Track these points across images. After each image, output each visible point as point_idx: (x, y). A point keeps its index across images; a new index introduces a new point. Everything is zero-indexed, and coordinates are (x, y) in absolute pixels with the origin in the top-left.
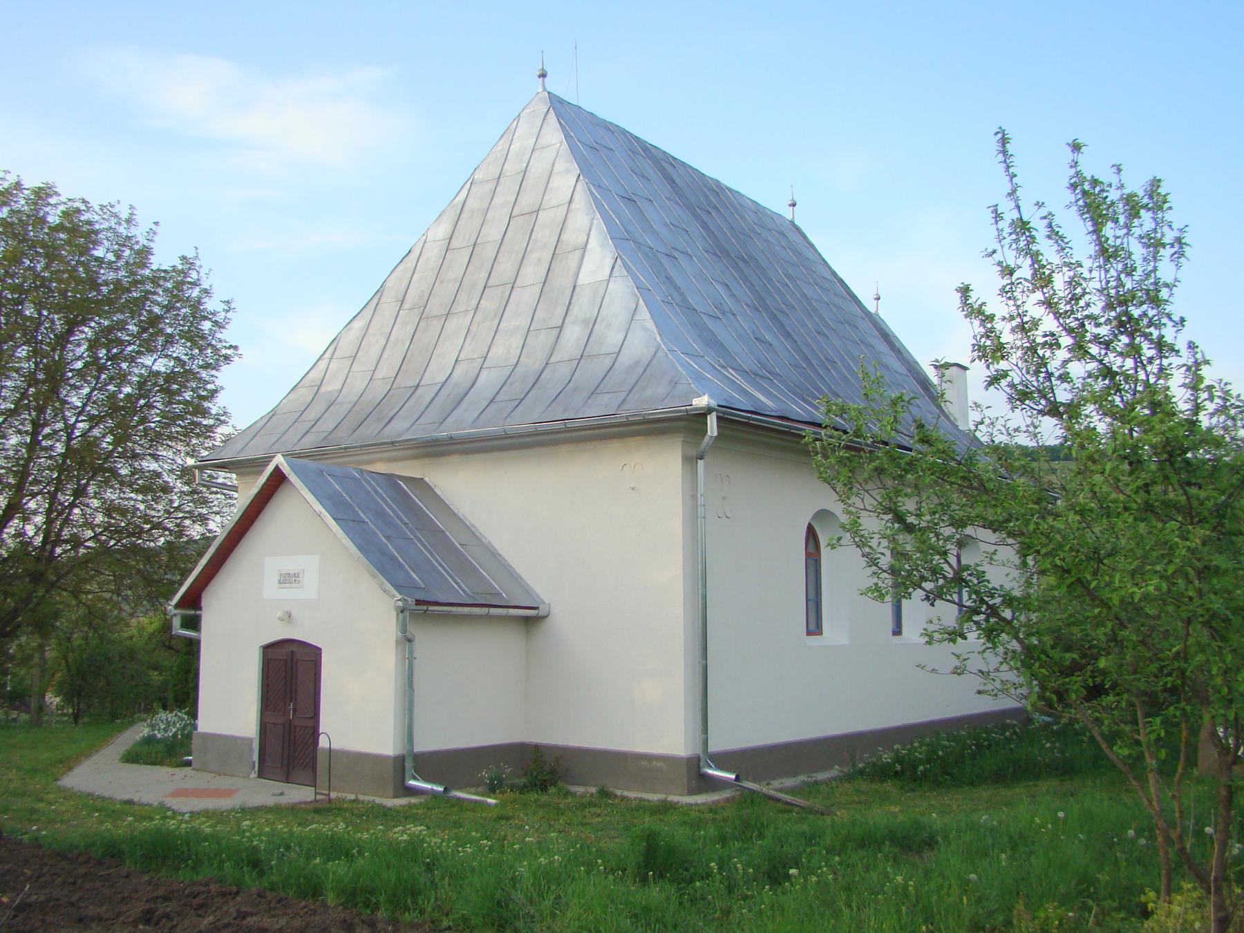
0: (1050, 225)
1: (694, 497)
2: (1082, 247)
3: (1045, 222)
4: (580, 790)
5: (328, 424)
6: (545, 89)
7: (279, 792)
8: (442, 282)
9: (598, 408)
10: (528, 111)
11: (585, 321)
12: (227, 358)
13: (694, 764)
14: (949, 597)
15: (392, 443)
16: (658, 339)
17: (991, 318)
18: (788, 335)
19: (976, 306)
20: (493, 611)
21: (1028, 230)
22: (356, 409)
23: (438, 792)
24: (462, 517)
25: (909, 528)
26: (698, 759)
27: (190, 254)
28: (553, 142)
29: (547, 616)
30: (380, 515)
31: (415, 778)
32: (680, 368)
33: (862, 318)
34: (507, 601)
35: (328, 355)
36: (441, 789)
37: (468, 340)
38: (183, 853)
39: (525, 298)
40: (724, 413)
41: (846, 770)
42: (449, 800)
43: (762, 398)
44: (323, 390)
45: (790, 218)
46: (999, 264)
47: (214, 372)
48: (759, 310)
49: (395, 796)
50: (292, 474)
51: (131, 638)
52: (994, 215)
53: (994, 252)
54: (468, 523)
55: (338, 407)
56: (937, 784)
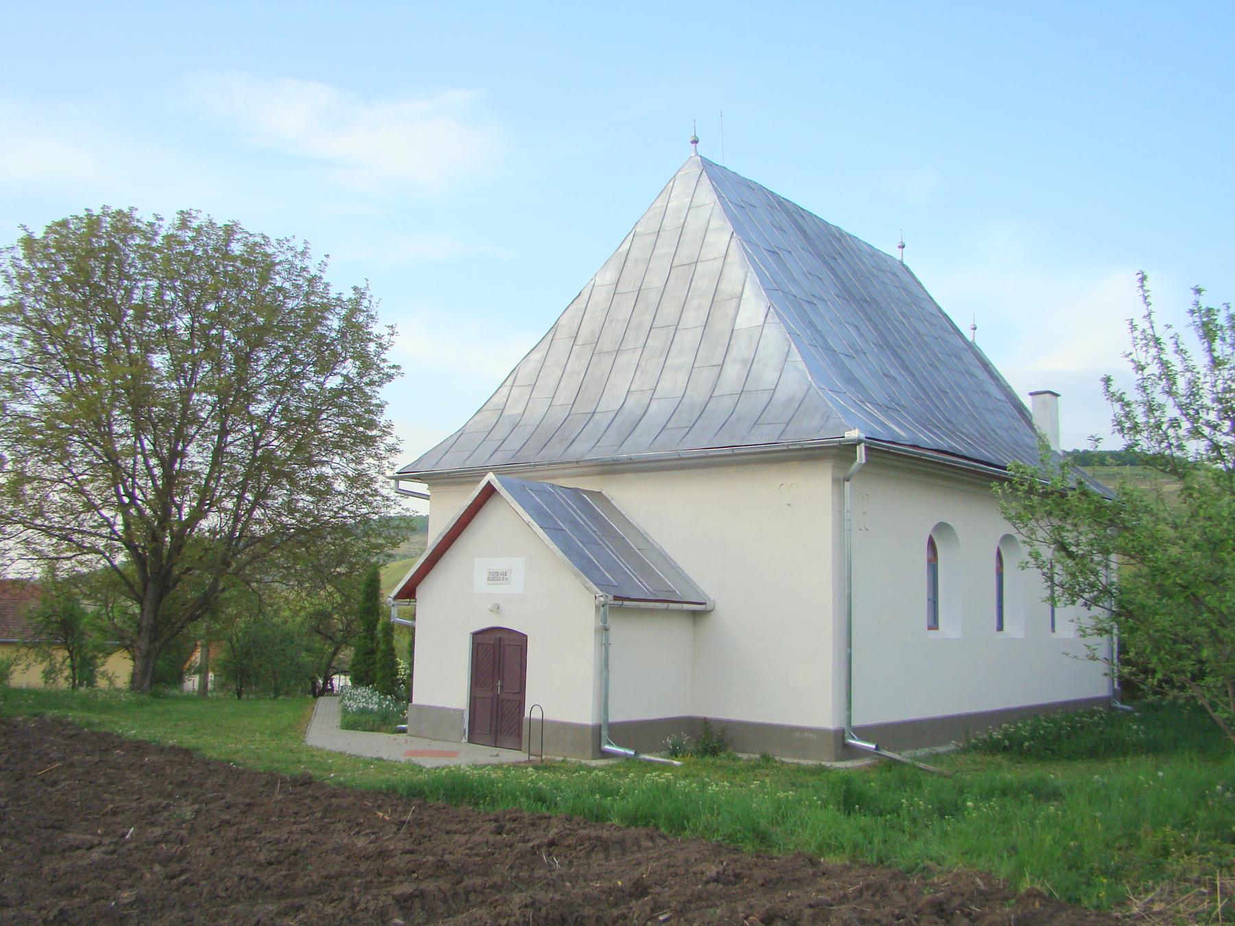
0: (1176, 343)
1: (841, 512)
2: (1200, 360)
3: (1173, 340)
4: (745, 756)
5: (515, 443)
6: (697, 154)
7: (496, 753)
8: (611, 322)
9: (762, 436)
10: (683, 173)
11: (744, 361)
12: (390, 377)
13: (840, 735)
14: (1101, 604)
15: (577, 462)
16: (810, 378)
17: (1128, 404)
18: (907, 370)
19: (1118, 394)
20: (672, 606)
21: (1160, 344)
22: (539, 431)
23: (630, 755)
24: (636, 526)
25: (1071, 555)
26: (843, 731)
27: (361, 285)
28: (707, 202)
30: (574, 523)
31: (609, 744)
32: (830, 404)
33: (966, 350)
34: (681, 598)
35: (509, 382)
36: (632, 753)
37: (638, 373)
38: (478, 791)
39: (687, 339)
40: (870, 444)
41: (961, 745)
42: (641, 761)
43: (897, 430)
44: (506, 413)
45: (899, 258)
46: (1132, 361)
47: (378, 389)
48: (882, 348)
49: (594, 758)
50: (503, 488)
51: (286, 622)
52: (1130, 326)
53: (1131, 354)
54: (642, 531)
55: (522, 428)
56: (1041, 759)
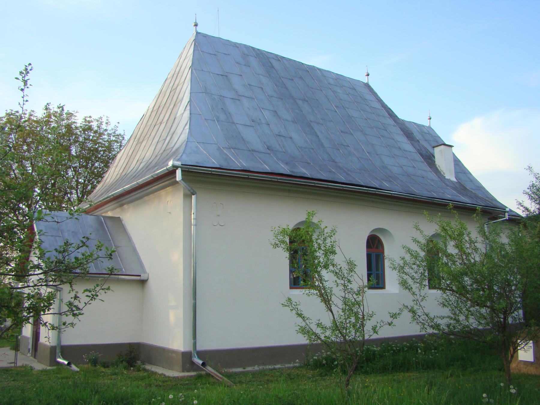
29: (148, 280)
36: (66, 362)
45: (366, 82)
